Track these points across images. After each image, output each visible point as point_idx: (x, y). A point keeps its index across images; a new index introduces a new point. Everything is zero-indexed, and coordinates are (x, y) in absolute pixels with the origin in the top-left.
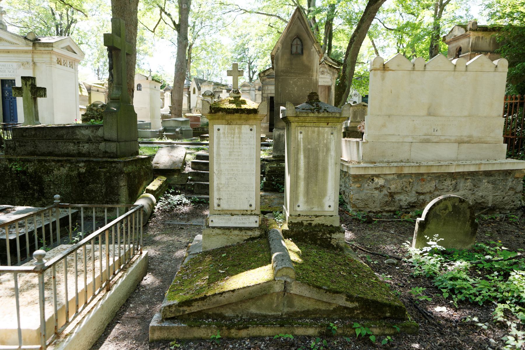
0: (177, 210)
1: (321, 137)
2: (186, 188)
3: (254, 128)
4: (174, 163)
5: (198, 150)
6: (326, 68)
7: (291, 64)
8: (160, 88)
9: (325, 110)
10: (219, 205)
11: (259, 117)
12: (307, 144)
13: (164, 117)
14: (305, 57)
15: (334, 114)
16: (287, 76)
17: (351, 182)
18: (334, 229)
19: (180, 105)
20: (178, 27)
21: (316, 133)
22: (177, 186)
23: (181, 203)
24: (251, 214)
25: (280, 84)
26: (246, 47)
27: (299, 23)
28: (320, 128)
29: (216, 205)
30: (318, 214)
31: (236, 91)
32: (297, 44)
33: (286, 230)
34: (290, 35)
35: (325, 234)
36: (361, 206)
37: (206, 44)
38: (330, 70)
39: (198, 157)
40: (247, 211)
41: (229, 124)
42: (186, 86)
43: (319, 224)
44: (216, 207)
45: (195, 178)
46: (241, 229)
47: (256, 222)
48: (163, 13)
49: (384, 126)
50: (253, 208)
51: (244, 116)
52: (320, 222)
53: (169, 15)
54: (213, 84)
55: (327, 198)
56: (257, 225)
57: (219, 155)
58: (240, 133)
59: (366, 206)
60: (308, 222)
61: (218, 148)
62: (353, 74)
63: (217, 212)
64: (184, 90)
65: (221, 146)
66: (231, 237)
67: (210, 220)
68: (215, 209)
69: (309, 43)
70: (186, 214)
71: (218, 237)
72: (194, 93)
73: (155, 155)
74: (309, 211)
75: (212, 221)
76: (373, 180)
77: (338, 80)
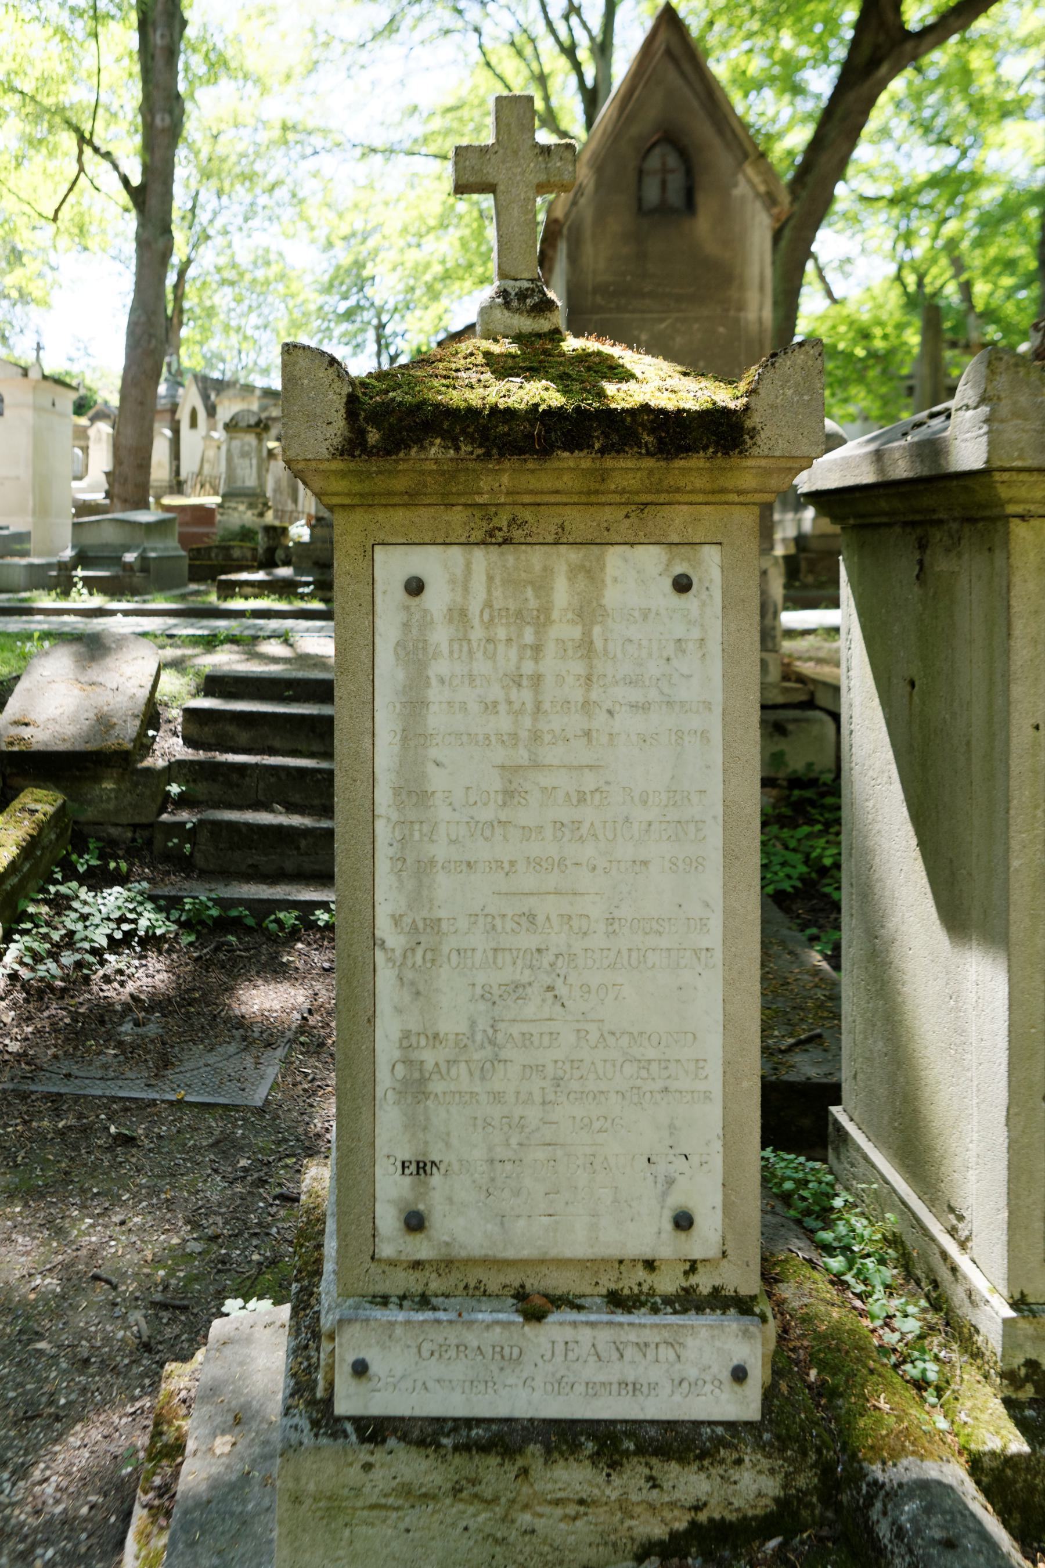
0: (107, 979)
2: (158, 845)
3: (710, 566)
4: (104, 723)
5: (210, 643)
8: (70, 408)
10: (415, 1222)
11: (748, 480)
13: (84, 508)
14: (703, 224)
19: (144, 465)
20: (139, 196)
22: (114, 831)
23: (129, 935)
24: (687, 1302)
26: (366, 273)
27: (672, 75)
29: (388, 1220)
31: (522, 296)
32: (665, 170)
34: (634, 130)
37: (234, 265)
39: (215, 684)
40: (650, 1265)
41: (495, 538)
42: (162, 403)
44: (392, 1239)
45: (202, 789)
46: (609, 1442)
47: (739, 1374)
48: (88, 150)
50: (706, 1238)
51: (629, 471)
53: (107, 155)
56: (743, 1405)
57: (414, 793)
58: (589, 611)
61: (413, 734)
63: (401, 1281)
64: (157, 417)
65: (436, 719)
66: (526, 1519)
67: (346, 1356)
68: (386, 1251)
69: (722, 158)
70: (149, 1010)
71: (410, 1518)
72: (194, 424)
73: (18, 678)
75: (360, 1369)
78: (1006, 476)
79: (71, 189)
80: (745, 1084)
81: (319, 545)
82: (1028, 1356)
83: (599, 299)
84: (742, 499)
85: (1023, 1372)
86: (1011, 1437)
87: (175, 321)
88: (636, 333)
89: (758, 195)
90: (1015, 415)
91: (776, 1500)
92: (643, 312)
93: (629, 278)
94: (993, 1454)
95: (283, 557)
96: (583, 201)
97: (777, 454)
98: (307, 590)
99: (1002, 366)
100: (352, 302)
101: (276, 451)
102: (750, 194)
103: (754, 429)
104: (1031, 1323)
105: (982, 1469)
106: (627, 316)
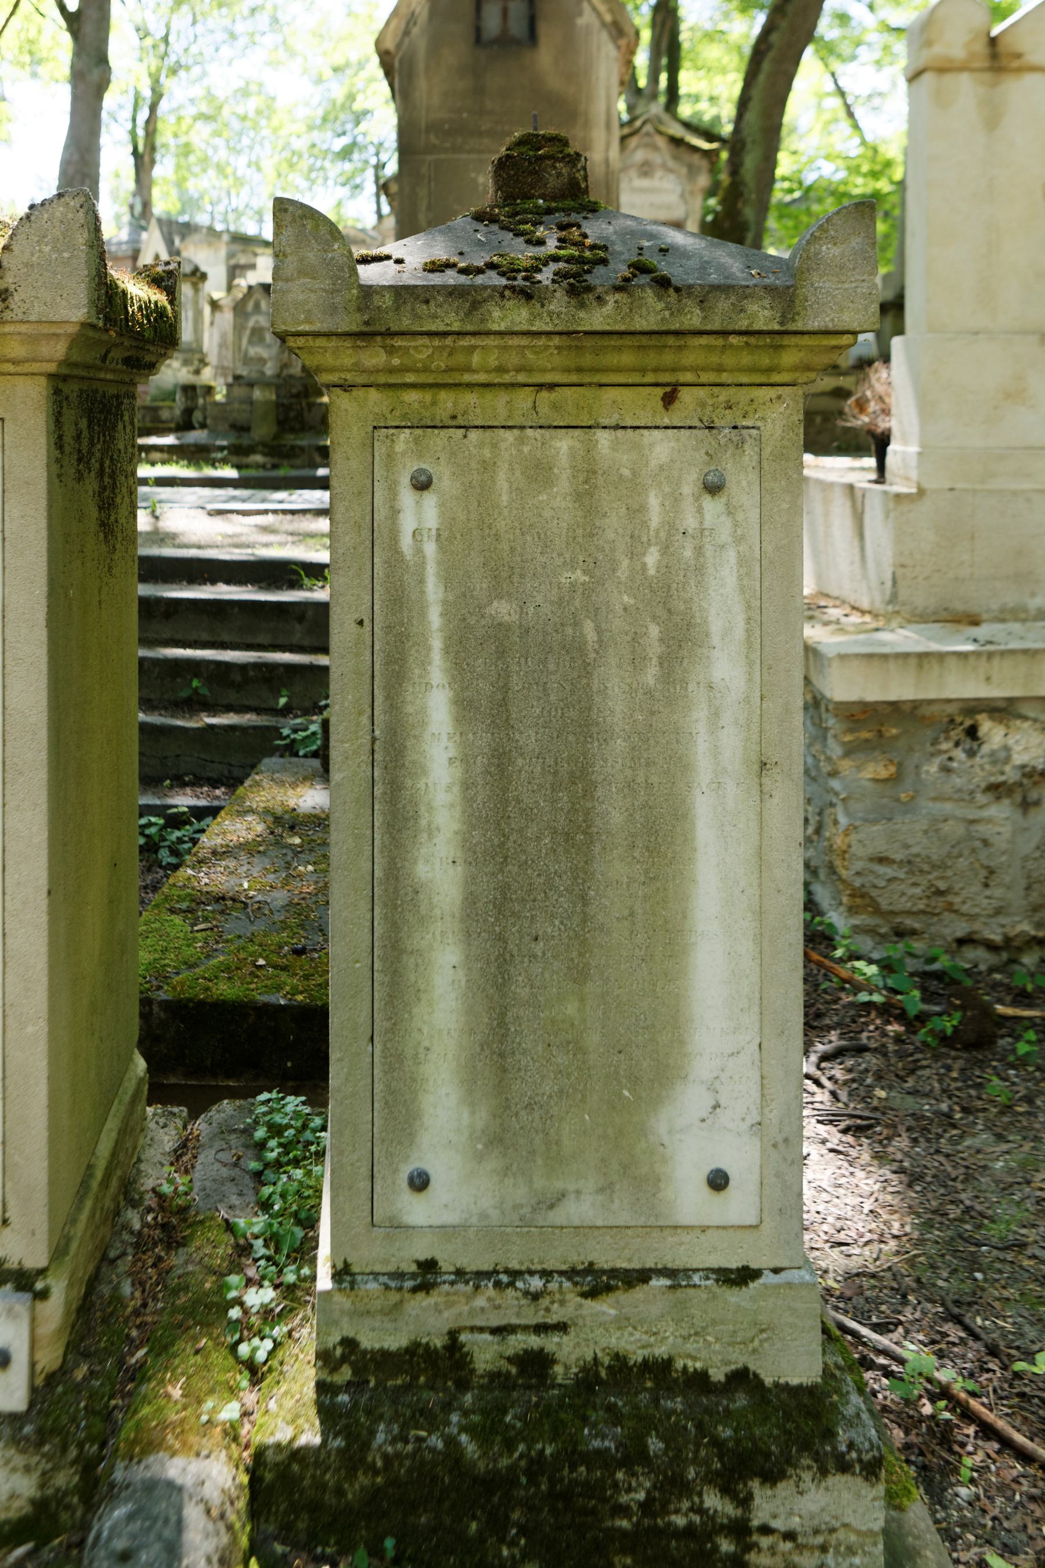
1: (613, 524)
6: (655, 148)
7: (479, 91)
9: (640, 268)
12: (481, 585)
14: (545, 57)
15: (723, 304)
16: (455, 149)
17: (835, 750)
18: (767, 1433)
21: (564, 483)
25: (422, 192)
28: (603, 438)
30: (607, 1258)
33: (298, 1455)
35: (685, 1489)
36: (904, 904)
38: (676, 158)
43: (619, 1360)
49: (1015, 394)
52: (635, 1345)
54: (226, 238)
55: (690, 1101)
59: (939, 902)
60: (519, 1342)
62: (772, 180)
74: (524, 1223)
76: (972, 732)
77: (712, 202)
78: (301, 342)
79: (12, 14)
80: (30, 1029)
81: (236, 406)
82: (345, 1333)
83: (433, 139)
84: (18, 369)
85: (339, 1352)
86: (306, 1426)
87: (146, 159)
88: (473, 175)
89: (604, 24)
90: (301, 273)
91: (33, 1502)
92: (480, 152)
93: (465, 115)
94: (278, 1446)
95: (201, 419)
96: (415, 31)
97: (33, 318)
98: (219, 455)
99: (288, 217)
100: (345, 141)
101: (221, 303)
102: (596, 23)
103: (7, 290)
104: (348, 1297)
105: (265, 1464)
106: (464, 156)
